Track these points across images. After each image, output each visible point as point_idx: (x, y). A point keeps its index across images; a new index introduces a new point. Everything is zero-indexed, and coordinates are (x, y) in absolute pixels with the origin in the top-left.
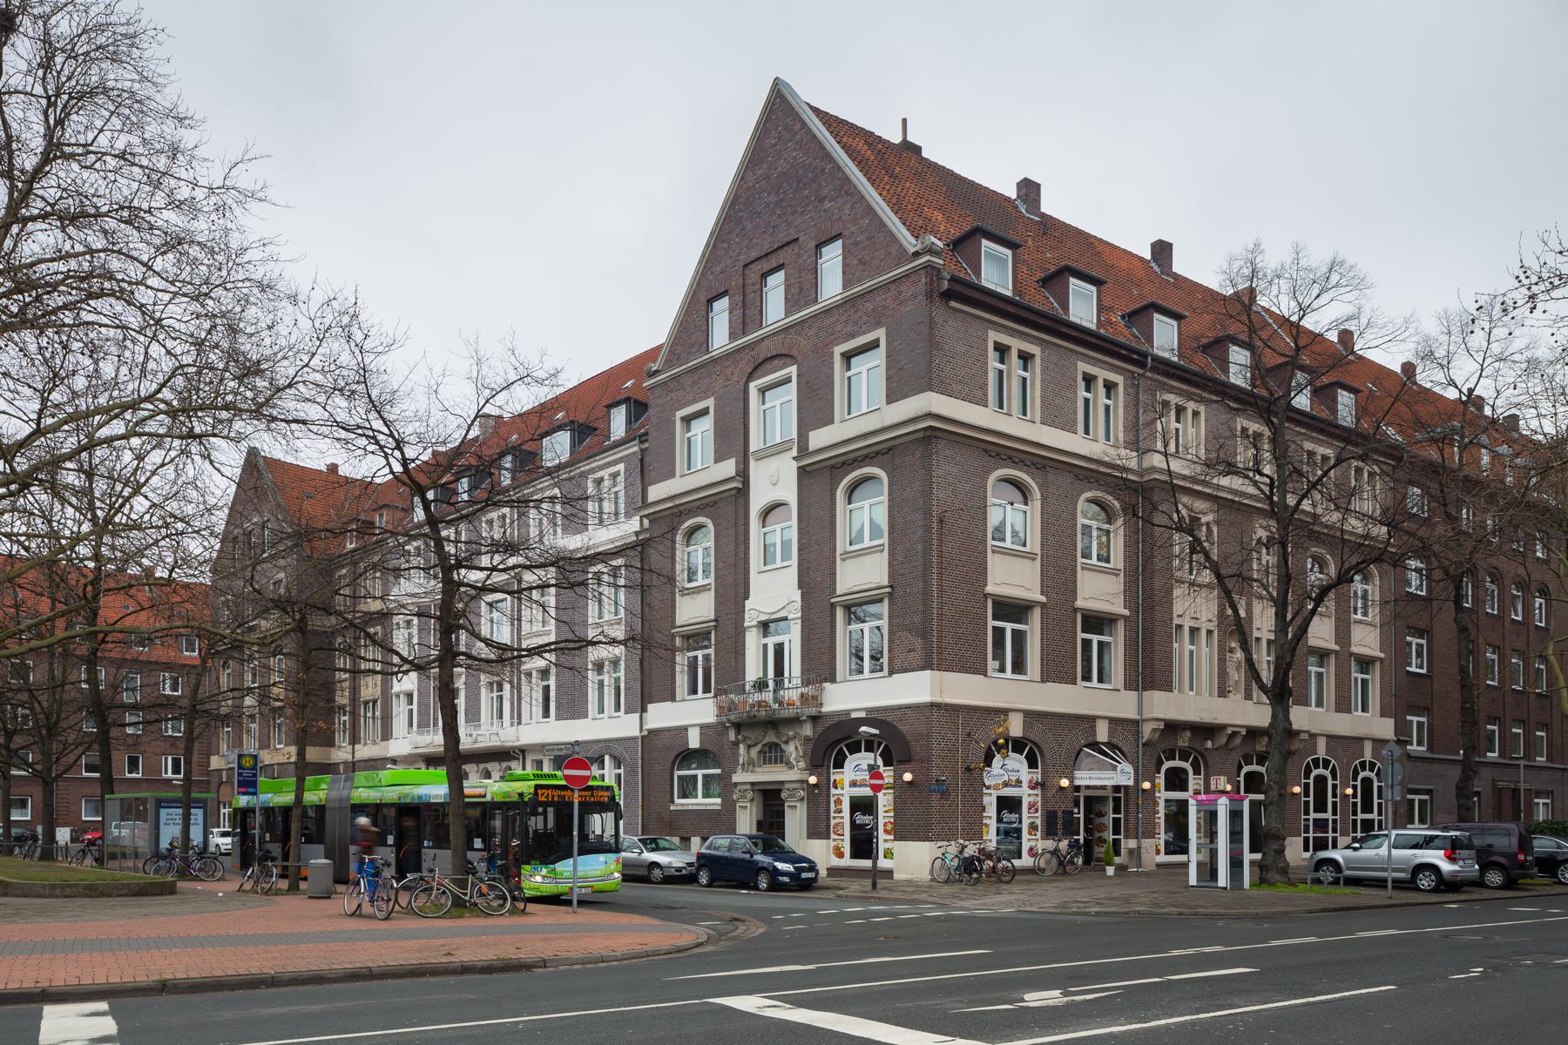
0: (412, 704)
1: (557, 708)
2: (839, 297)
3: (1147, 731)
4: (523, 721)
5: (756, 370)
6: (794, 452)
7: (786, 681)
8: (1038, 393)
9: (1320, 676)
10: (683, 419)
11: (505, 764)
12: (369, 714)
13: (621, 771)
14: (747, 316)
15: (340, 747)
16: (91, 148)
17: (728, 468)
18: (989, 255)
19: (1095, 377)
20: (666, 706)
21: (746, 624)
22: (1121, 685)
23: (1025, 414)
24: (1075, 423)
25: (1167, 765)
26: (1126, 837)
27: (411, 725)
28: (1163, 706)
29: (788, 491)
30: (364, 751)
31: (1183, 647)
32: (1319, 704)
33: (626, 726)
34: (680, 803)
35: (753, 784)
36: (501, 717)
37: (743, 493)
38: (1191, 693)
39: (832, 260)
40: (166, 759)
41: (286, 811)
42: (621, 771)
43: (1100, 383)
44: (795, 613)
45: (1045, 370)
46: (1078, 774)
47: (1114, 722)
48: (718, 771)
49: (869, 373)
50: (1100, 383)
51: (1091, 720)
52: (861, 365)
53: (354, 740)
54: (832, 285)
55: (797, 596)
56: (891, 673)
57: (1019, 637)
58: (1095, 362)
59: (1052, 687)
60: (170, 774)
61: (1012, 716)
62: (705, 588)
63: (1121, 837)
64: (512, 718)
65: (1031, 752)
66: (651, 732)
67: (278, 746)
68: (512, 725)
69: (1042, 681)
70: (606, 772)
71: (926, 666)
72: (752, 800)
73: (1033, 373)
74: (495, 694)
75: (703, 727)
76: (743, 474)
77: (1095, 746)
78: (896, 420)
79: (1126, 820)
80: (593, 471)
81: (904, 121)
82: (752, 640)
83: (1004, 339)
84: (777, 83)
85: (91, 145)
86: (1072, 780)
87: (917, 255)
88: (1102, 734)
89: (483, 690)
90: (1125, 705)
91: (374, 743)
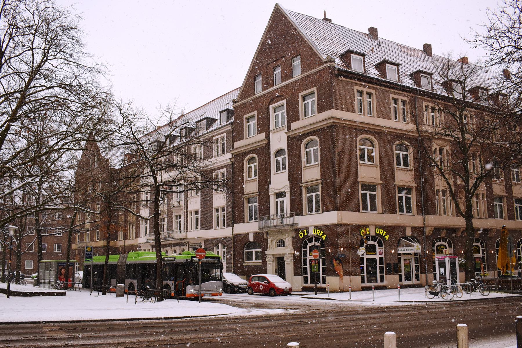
0: (147, 224)
1: (201, 225)
2: (300, 76)
3: (427, 231)
4: (188, 231)
5: (271, 102)
6: (286, 131)
7: (285, 215)
8: (375, 107)
9: (501, 206)
10: (246, 118)
11: (182, 247)
12: (131, 228)
13: (225, 250)
14: (268, 83)
15: (120, 241)
16: (56, 57)
17: (263, 136)
18: (354, 59)
19: (398, 99)
20: (241, 225)
21: (270, 194)
22: (415, 213)
23: (371, 114)
24: (391, 116)
25: (437, 244)
26: (421, 273)
27: (146, 233)
28: (433, 220)
29: (284, 145)
30: (129, 242)
31: (439, 197)
32: (501, 217)
33: (226, 232)
34: (247, 262)
35: (273, 255)
36: (180, 229)
37: (268, 145)
38: (444, 215)
39: (297, 62)
40: (55, 245)
41: (102, 266)
42: (225, 250)
43: (400, 101)
44: (287, 190)
45: (377, 98)
46: (399, 248)
47: (413, 229)
48: (261, 250)
49: (312, 101)
50: (400, 101)
51: (404, 227)
52: (309, 101)
53: (125, 238)
54: (298, 75)
55: (288, 183)
56: (323, 212)
57: (373, 197)
58: (397, 94)
59: (385, 215)
60: (56, 251)
61: (371, 227)
62: (254, 180)
63: (419, 273)
64: (184, 229)
65: (380, 240)
66: (236, 235)
67: (97, 241)
68: (184, 232)
69: (383, 213)
70: (219, 250)
71: (336, 209)
72: (273, 261)
73: (373, 100)
74: (178, 220)
75: (255, 233)
76: (268, 137)
77: (406, 238)
78: (321, 119)
79: (421, 266)
80: (215, 136)
81: (325, 11)
82: (272, 200)
83: (361, 89)
84: (277, 5)
85: (56, 55)
86: (396, 250)
87: (326, 62)
88: (409, 233)
89: (174, 219)
90: (417, 221)
91: (133, 239)
